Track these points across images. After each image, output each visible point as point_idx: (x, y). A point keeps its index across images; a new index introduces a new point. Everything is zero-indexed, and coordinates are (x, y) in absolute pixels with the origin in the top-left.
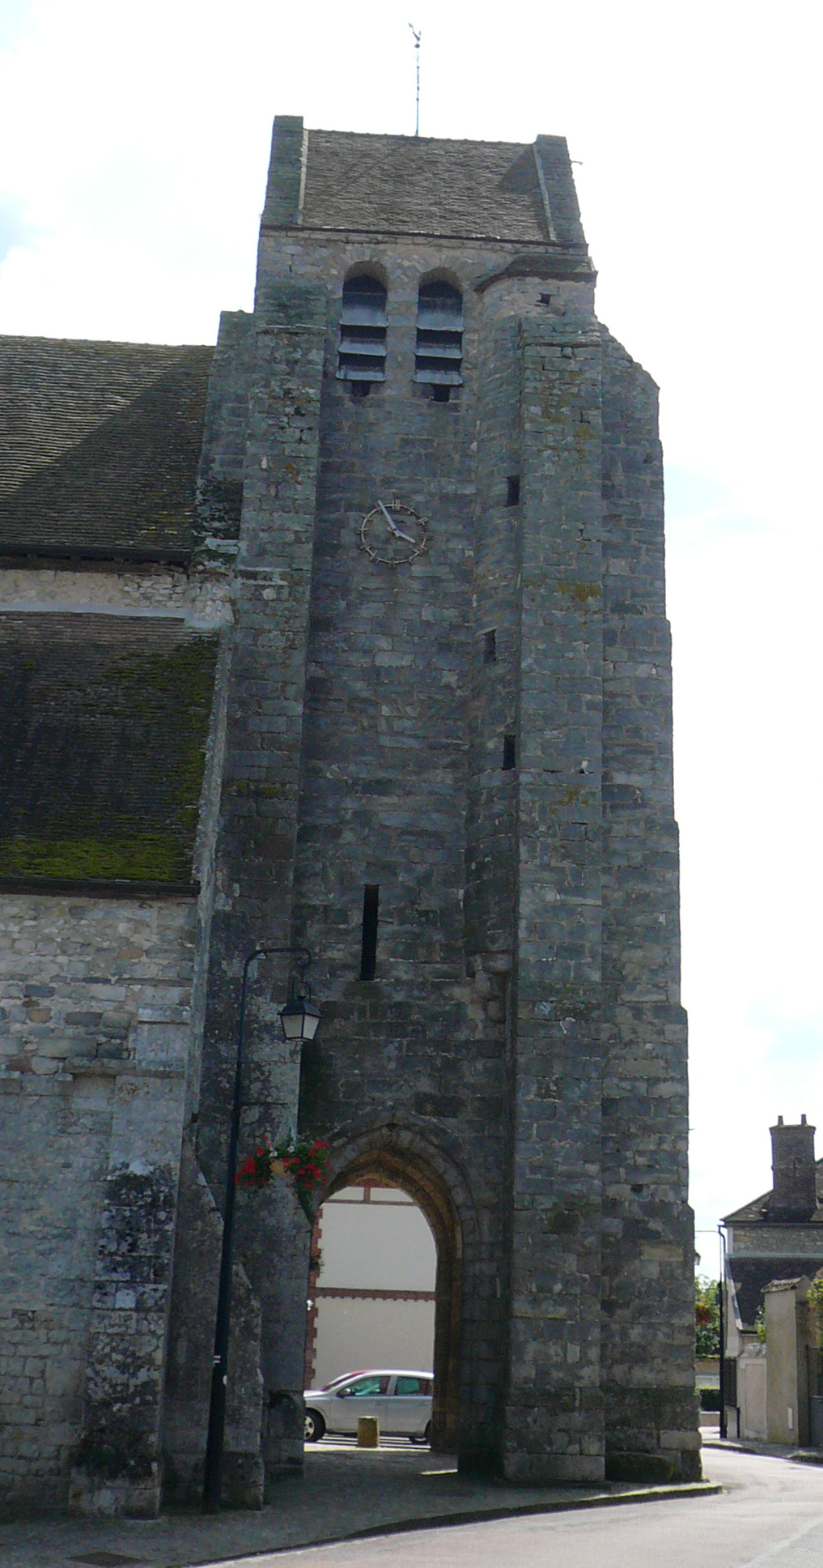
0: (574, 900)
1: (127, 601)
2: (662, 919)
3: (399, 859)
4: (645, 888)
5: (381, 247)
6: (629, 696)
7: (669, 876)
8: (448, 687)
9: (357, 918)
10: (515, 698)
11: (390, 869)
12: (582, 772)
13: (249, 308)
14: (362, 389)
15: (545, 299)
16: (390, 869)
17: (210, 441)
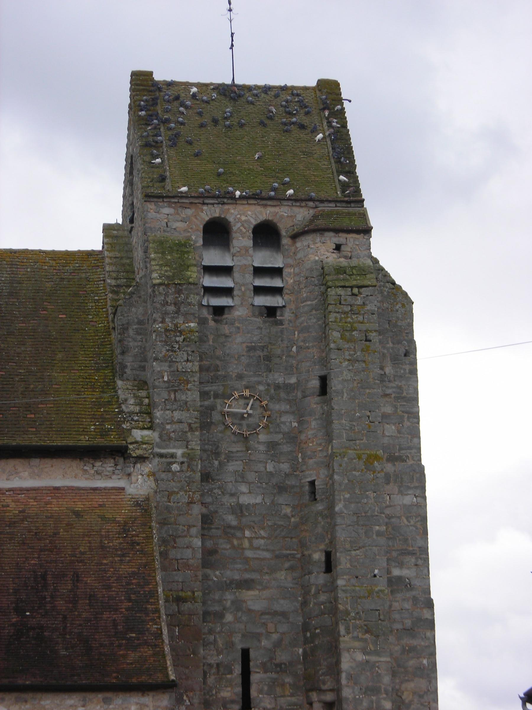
0: (373, 658)
1: (87, 476)
2: (425, 662)
3: (262, 630)
4: (414, 642)
5: (226, 207)
6: (399, 518)
7: (428, 634)
8: (286, 515)
9: (237, 669)
10: (332, 527)
11: (257, 637)
12: (375, 576)
13: (120, 221)
14: (219, 311)
15: (338, 248)
16: (257, 637)
17: (123, 353)
